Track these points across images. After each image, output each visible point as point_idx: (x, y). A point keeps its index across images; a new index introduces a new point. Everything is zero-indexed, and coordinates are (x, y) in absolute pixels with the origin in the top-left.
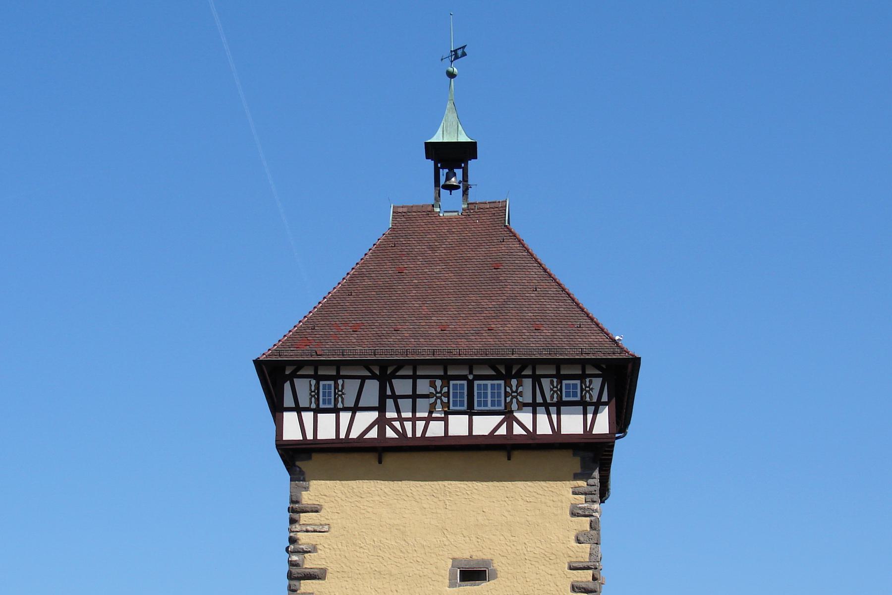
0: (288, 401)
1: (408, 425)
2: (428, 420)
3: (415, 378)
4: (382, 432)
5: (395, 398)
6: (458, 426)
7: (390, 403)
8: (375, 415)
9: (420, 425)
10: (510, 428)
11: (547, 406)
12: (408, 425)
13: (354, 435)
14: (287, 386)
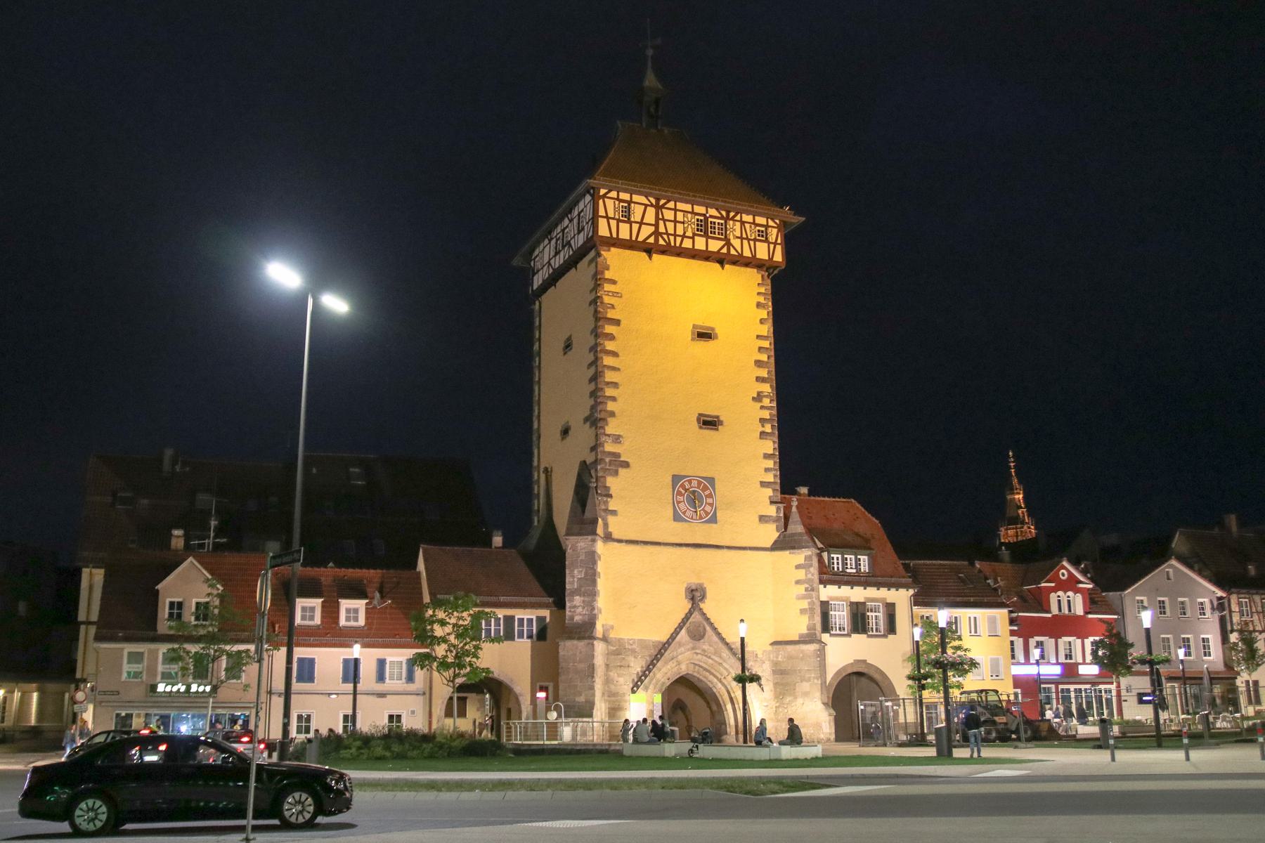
0: (602, 212)
1: (672, 238)
2: (684, 236)
3: (675, 210)
4: (657, 240)
5: (665, 221)
6: (700, 244)
7: (661, 223)
8: (652, 229)
9: (679, 239)
10: (729, 250)
11: (749, 240)
12: (672, 238)
13: (640, 239)
14: (601, 202)
